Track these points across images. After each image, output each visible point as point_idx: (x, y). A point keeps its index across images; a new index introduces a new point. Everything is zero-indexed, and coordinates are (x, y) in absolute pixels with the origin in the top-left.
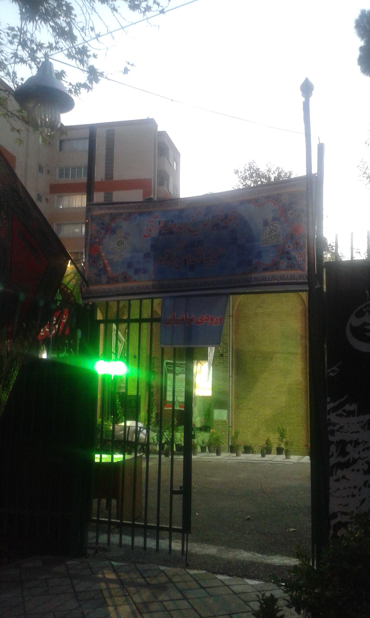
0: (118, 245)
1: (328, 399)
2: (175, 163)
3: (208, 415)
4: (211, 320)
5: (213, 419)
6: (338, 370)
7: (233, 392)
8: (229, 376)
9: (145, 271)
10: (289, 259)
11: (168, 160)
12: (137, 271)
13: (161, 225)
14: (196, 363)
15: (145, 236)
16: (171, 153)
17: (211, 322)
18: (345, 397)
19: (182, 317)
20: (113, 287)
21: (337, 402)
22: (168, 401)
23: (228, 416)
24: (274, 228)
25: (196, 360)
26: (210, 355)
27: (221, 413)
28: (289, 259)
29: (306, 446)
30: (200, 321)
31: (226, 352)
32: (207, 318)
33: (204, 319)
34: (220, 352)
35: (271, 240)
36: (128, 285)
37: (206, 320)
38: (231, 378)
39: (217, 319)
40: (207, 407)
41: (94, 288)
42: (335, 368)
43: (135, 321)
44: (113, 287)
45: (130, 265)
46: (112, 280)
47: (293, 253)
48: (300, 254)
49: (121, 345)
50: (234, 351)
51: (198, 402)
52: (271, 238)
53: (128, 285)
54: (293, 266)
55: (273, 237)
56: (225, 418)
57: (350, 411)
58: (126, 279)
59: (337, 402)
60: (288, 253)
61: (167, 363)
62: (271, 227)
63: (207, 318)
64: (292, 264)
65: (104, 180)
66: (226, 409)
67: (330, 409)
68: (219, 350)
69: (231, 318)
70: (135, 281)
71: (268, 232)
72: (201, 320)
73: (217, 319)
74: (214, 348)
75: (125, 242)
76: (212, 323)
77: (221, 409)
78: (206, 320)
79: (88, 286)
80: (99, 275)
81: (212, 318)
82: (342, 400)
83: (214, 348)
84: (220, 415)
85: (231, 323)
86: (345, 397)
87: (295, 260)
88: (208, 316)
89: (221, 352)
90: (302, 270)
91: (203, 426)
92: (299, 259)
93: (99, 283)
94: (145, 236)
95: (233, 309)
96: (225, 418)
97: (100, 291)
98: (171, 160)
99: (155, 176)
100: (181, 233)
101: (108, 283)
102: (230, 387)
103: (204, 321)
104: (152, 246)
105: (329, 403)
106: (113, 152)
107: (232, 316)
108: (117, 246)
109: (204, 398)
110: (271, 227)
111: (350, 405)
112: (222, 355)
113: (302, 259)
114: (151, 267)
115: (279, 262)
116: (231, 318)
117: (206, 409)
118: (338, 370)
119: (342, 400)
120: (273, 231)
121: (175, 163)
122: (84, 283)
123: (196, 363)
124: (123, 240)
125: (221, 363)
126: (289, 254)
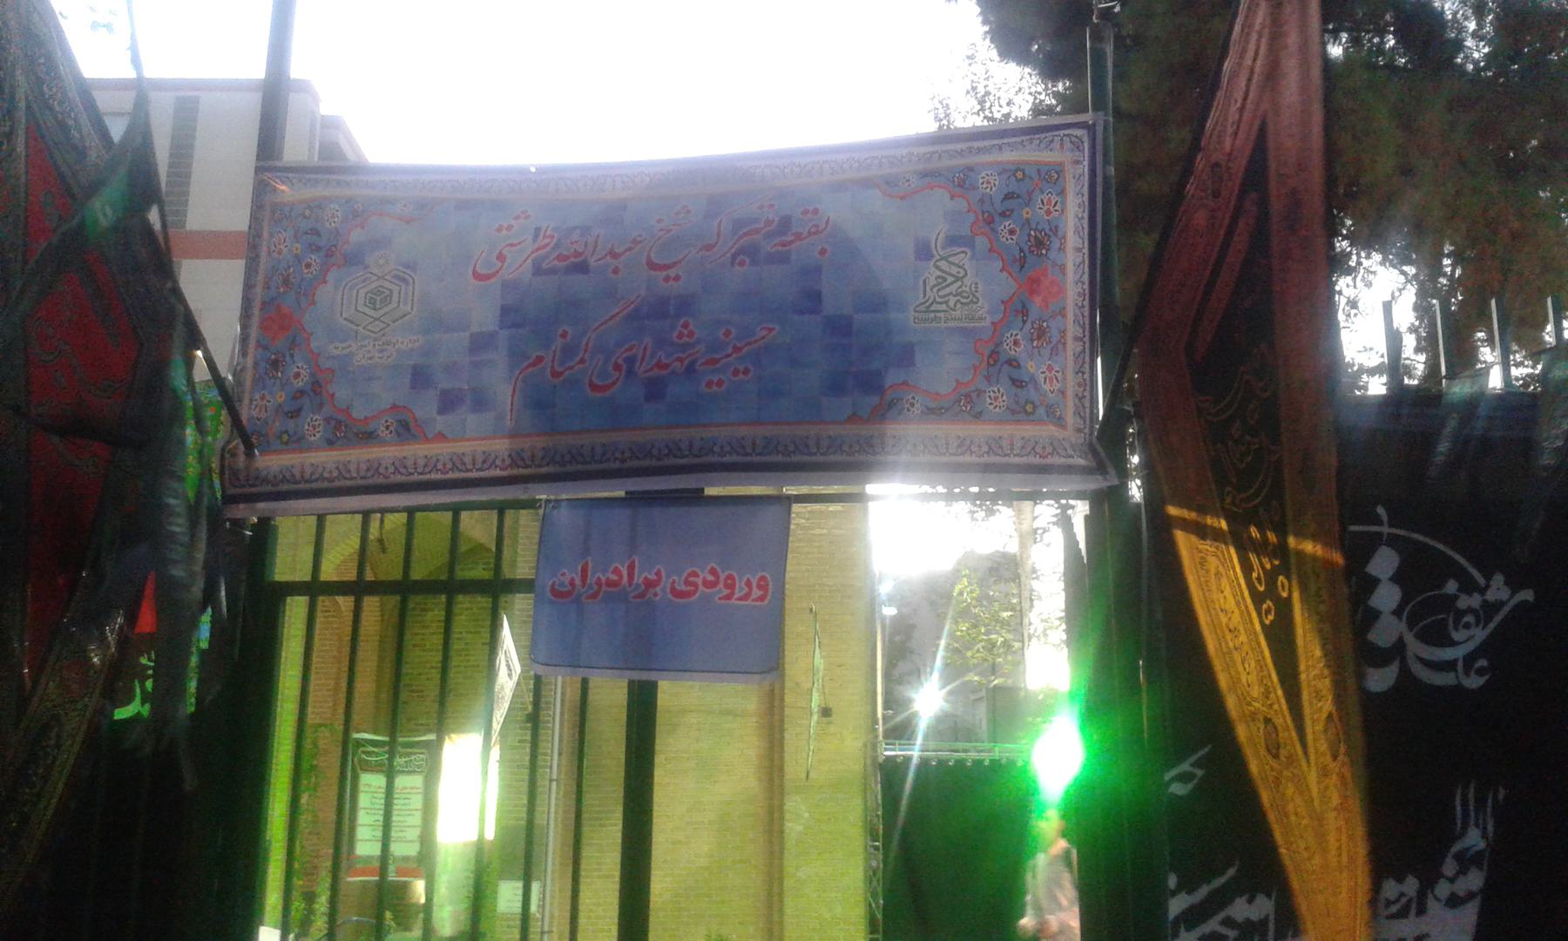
0: (373, 302)
1: (1172, 881)
4: (726, 586)
6: (1200, 773)
9: (481, 402)
10: (1018, 383)
12: (448, 403)
13: (541, 242)
15: (477, 276)
17: (726, 592)
18: (1231, 872)
19: (617, 571)
20: (357, 457)
21: (1204, 891)
24: (954, 270)
28: (1018, 383)
30: (683, 588)
32: (710, 578)
33: (699, 581)
35: (944, 307)
36: (417, 451)
37: (706, 584)
39: (749, 583)
41: (271, 463)
42: (1185, 767)
43: (428, 587)
44: (357, 457)
45: (420, 378)
46: (345, 431)
47: (1031, 367)
48: (1050, 368)
52: (946, 303)
53: (417, 451)
54: (1029, 408)
55: (952, 300)
57: (1248, 921)
58: (406, 429)
59: (1204, 891)
60: (1013, 363)
62: (943, 264)
63: (710, 578)
64: (1027, 402)
67: (1177, 918)
70: (441, 437)
71: (932, 281)
72: (687, 583)
73: (749, 583)
74: (1491, 385)
75: (395, 295)
76: (728, 597)
78: (706, 584)
79: (249, 453)
80: (295, 414)
81: (730, 577)
82: (1218, 882)
83: (1491, 385)
86: (1231, 872)
87: (1037, 388)
88: (713, 572)
90: (1060, 422)
92: (1047, 387)
93: (295, 442)
94: (477, 276)
97: (302, 472)
100: (616, 271)
101: (331, 443)
103: (701, 588)
104: (505, 311)
105: (1174, 893)
108: (367, 310)
110: (943, 264)
111: (1250, 901)
113: (1057, 386)
114: (502, 386)
115: (980, 393)
118: (1200, 773)
119: (1218, 882)
120: (950, 279)
122: (237, 441)
124: (387, 285)
126: (1019, 366)
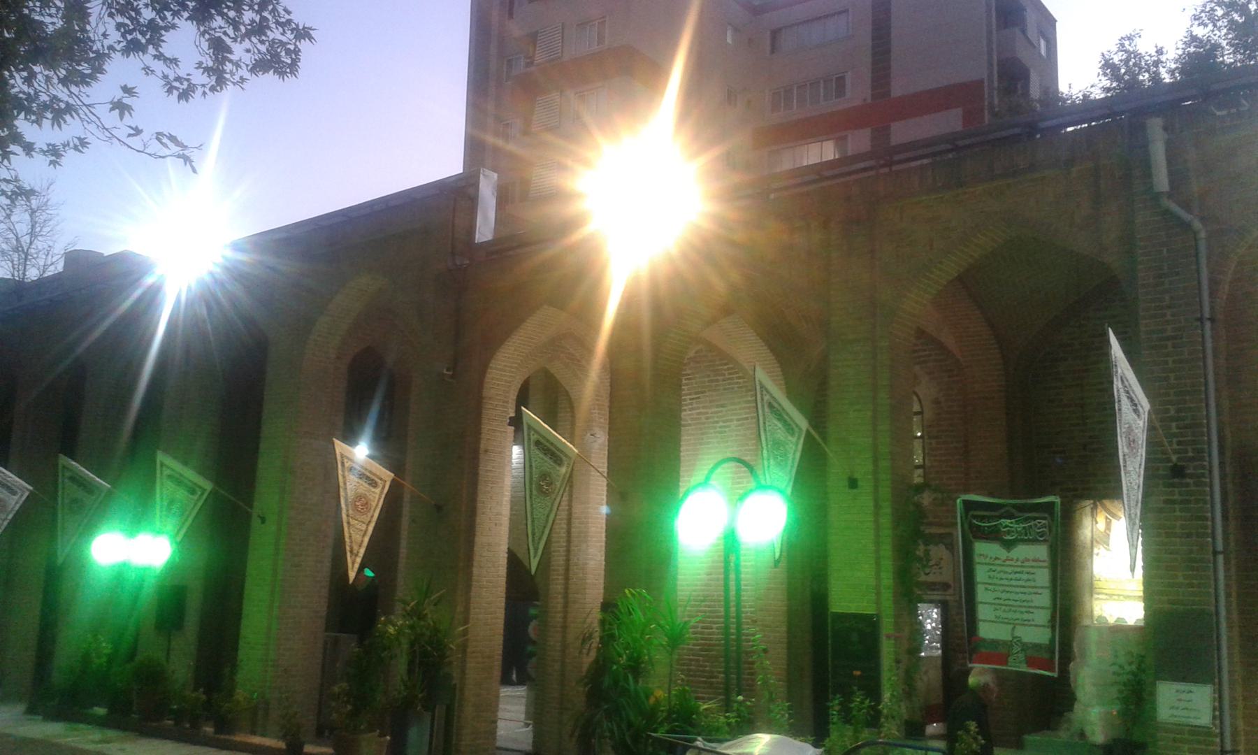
2: (1043, 43)
3: (1135, 698)
5: (1154, 718)
7: (1235, 616)
8: (1215, 553)
11: (1024, 32)
14: (1088, 510)
16: (1031, 18)
22: (984, 640)
23: (1218, 710)
25: (1089, 498)
26: (1130, 468)
27: (1183, 696)
29: (585, 162)
31: (1192, 459)
34: (1169, 460)
38: (1220, 558)
40: (1128, 668)
49: (794, 440)
50: (1228, 454)
51: (1093, 648)
56: (1205, 719)
61: (968, 505)
65: (869, 101)
66: (1204, 682)
68: (1164, 453)
69: (1208, 325)
77: (1184, 679)
84: (1184, 704)
85: (1209, 345)
89: (1174, 458)
91: (1116, 741)
95: (1212, 294)
96: (1205, 719)
98: (1032, 32)
99: (990, 75)
102: (1221, 593)
106: (889, 34)
107: (1212, 320)
109: (1118, 630)
112: (1178, 471)
116: (1208, 325)
117: (1125, 678)
121: (1043, 43)
123: (1088, 510)
125: (1173, 502)
